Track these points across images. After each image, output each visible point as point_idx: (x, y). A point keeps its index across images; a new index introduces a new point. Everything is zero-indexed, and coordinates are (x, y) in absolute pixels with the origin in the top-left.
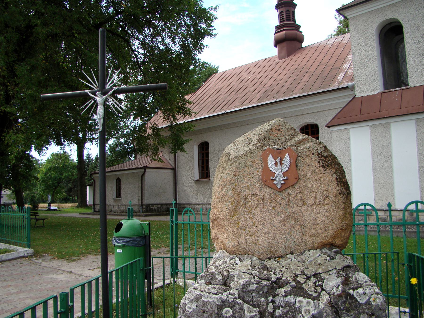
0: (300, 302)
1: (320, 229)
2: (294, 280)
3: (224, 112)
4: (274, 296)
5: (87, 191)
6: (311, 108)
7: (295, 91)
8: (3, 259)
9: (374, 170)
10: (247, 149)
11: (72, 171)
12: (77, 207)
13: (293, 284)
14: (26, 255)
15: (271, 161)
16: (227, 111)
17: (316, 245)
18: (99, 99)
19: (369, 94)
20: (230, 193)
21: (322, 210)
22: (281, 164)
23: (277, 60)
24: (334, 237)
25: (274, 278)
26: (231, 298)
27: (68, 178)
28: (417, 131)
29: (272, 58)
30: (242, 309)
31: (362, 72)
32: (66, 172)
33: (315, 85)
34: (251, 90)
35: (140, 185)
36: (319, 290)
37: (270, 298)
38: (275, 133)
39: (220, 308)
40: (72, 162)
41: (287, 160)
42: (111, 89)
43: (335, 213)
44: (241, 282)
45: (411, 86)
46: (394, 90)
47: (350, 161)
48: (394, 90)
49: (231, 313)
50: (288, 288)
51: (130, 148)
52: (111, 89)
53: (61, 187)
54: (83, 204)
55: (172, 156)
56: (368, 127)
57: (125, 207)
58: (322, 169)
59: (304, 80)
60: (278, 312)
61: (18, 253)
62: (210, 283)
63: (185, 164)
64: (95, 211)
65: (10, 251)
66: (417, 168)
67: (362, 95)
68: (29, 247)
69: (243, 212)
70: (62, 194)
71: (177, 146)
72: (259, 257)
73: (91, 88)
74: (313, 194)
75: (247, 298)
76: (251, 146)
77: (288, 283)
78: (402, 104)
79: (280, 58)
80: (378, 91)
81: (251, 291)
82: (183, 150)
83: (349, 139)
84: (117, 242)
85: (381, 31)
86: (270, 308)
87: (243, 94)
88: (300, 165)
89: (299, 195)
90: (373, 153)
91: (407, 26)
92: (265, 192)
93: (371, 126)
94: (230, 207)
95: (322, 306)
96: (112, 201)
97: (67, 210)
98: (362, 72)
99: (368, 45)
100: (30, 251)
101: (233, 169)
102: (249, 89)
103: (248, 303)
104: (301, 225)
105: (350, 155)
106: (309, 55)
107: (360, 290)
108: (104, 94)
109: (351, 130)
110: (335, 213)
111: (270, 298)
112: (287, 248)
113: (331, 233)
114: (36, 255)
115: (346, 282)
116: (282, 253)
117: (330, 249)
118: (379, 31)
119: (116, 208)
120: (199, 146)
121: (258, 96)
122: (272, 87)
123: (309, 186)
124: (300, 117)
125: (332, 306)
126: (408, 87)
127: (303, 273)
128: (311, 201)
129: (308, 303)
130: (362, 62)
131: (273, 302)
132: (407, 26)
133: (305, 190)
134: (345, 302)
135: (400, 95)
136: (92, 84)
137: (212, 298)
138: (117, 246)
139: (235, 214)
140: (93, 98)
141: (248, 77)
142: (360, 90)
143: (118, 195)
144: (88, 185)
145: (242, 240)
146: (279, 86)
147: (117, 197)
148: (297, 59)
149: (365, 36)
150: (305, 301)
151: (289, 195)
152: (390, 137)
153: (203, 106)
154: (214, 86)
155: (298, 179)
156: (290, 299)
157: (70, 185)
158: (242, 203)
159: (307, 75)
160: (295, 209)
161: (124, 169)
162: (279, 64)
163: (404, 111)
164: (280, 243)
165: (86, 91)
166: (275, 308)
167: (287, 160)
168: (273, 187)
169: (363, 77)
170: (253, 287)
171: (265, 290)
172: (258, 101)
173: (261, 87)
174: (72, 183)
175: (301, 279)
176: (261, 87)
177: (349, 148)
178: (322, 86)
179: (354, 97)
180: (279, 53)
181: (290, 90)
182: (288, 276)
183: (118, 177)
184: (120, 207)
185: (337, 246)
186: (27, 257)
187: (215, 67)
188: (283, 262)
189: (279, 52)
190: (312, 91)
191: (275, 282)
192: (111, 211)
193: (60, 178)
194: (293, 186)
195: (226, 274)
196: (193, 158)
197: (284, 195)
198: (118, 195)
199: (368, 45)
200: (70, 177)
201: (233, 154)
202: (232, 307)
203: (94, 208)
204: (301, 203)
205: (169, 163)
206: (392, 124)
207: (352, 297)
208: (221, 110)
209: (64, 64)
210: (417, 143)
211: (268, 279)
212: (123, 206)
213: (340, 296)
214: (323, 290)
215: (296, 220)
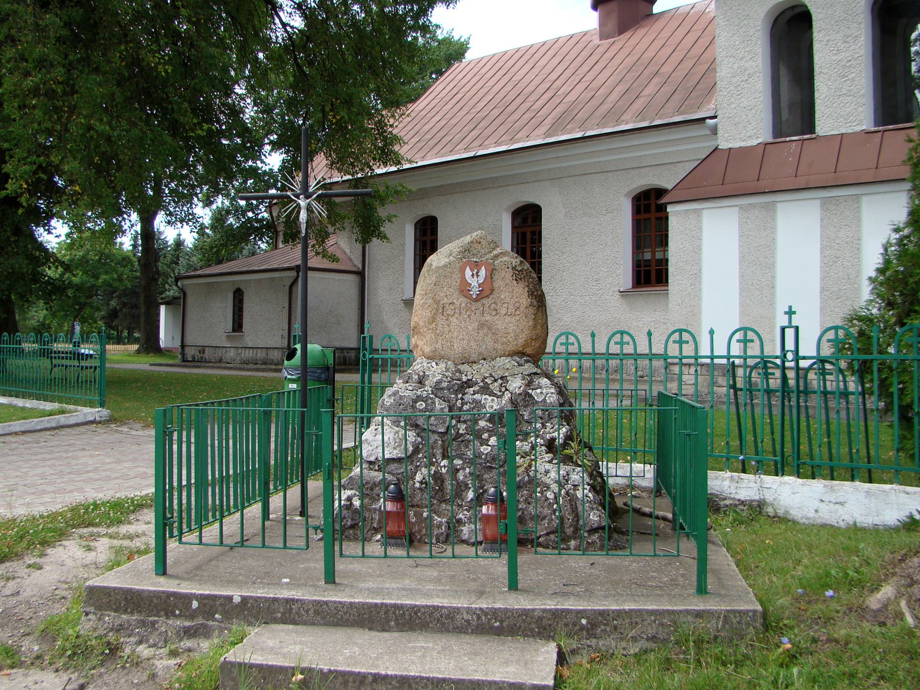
0: (485, 399)
1: (511, 337)
2: (483, 381)
3: (471, 154)
4: (463, 395)
5: (159, 315)
6: (656, 154)
7: (626, 117)
8: (61, 423)
9: (742, 290)
10: (447, 260)
11: (121, 269)
12: (138, 352)
13: (482, 384)
14: (98, 419)
15: (468, 272)
16: (480, 153)
17: (507, 353)
18: (303, 203)
19: (743, 144)
20: (430, 301)
21: (513, 320)
22: (478, 276)
23: (597, 41)
24: (524, 346)
25: (464, 379)
26: (425, 394)
27: (110, 285)
28: (822, 220)
29: (585, 34)
30: (434, 403)
31: (732, 100)
32: (107, 273)
33: (668, 105)
34: (533, 108)
35: (287, 305)
36: (503, 389)
37: (460, 396)
38: (476, 246)
39: (415, 402)
40: (121, 249)
41: (483, 272)
42: (314, 193)
43: (525, 323)
44: (435, 380)
45: (820, 134)
46: (788, 139)
47: (700, 271)
48: (788, 139)
49: (424, 405)
50: (476, 388)
51: (258, 221)
52: (314, 193)
53: (92, 307)
54: (151, 345)
55: (359, 246)
56: (736, 209)
57: (251, 351)
58: (515, 282)
59: (650, 90)
60: (465, 407)
61: (84, 414)
62: (407, 382)
63: (385, 262)
64: (184, 360)
65: (70, 412)
66: (818, 290)
67: (731, 146)
68: (102, 405)
69: (441, 320)
70: (95, 322)
71: (369, 229)
72: (454, 362)
73: (293, 190)
74: (506, 305)
75: (439, 394)
76: (451, 258)
77: (477, 383)
78: (800, 168)
79: (603, 36)
80: (760, 141)
81: (442, 389)
82: (383, 237)
83: (700, 228)
84: (289, 374)
85: (776, 21)
86: (459, 403)
87: (516, 116)
88: (495, 277)
89: (493, 306)
90: (742, 258)
91: (820, 16)
92: (462, 301)
93: (741, 207)
94: (429, 314)
95: (504, 402)
96: (224, 338)
97: (115, 358)
98: (732, 100)
99: (747, 49)
100: (104, 412)
101: (434, 279)
102: (529, 105)
103: (440, 398)
104: (493, 334)
105: (700, 259)
106: (666, 34)
107: (539, 391)
108: (307, 197)
109: (705, 213)
110: (525, 323)
111: (460, 396)
112: (480, 354)
113: (521, 341)
114: (111, 420)
115: (529, 384)
116: (476, 359)
117: (521, 358)
118: (772, 21)
119: (232, 353)
120: (416, 225)
121: (549, 121)
122: (579, 103)
123: (503, 297)
124: (633, 172)
125: (512, 403)
126: (814, 136)
127: (491, 375)
128: (503, 311)
129: (493, 400)
130: (734, 80)
131: (462, 399)
132: (820, 16)
133: (498, 301)
134: (524, 399)
135: (799, 151)
136: (292, 185)
137: (408, 393)
138: (289, 379)
139: (433, 322)
140: (296, 202)
141: (531, 76)
142: (726, 135)
143: (238, 326)
144: (162, 304)
145: (439, 346)
146: (595, 102)
147: (234, 330)
148: (639, 41)
149: (744, 29)
150: (490, 398)
151: (483, 305)
152: (773, 229)
153: (428, 137)
154: (455, 91)
155: (492, 290)
156: (477, 397)
157: (113, 303)
158: (440, 311)
159: (655, 81)
160: (488, 318)
161: (251, 269)
162: (600, 50)
163: (800, 182)
164: (474, 349)
165: (289, 193)
166: (463, 404)
167: (483, 272)
168: (469, 297)
169: (735, 111)
170: (445, 385)
171: (456, 388)
172: (547, 134)
173: (556, 100)
174: (119, 297)
175: (488, 381)
176: (556, 100)
177: (700, 248)
178: (683, 107)
179: (716, 148)
180: (601, 25)
181: (615, 114)
182: (477, 378)
183: (236, 287)
184: (240, 351)
185: (528, 356)
186: (100, 422)
187: (462, 40)
188: (475, 366)
189: (602, 23)
190: (660, 118)
191: (466, 382)
192: (220, 361)
193: (93, 286)
194: (487, 296)
195: (421, 374)
196: (403, 250)
197: (479, 304)
198: (238, 326)
199: (747, 49)
200: (116, 284)
201: (434, 264)
202: (425, 402)
203: (183, 353)
204: (494, 313)
205: (350, 260)
206: (779, 205)
207: (531, 396)
208: (466, 149)
209: (160, 67)
210: (822, 244)
211: (459, 380)
212: (247, 350)
213: (520, 394)
214: (507, 390)
215: (489, 328)
